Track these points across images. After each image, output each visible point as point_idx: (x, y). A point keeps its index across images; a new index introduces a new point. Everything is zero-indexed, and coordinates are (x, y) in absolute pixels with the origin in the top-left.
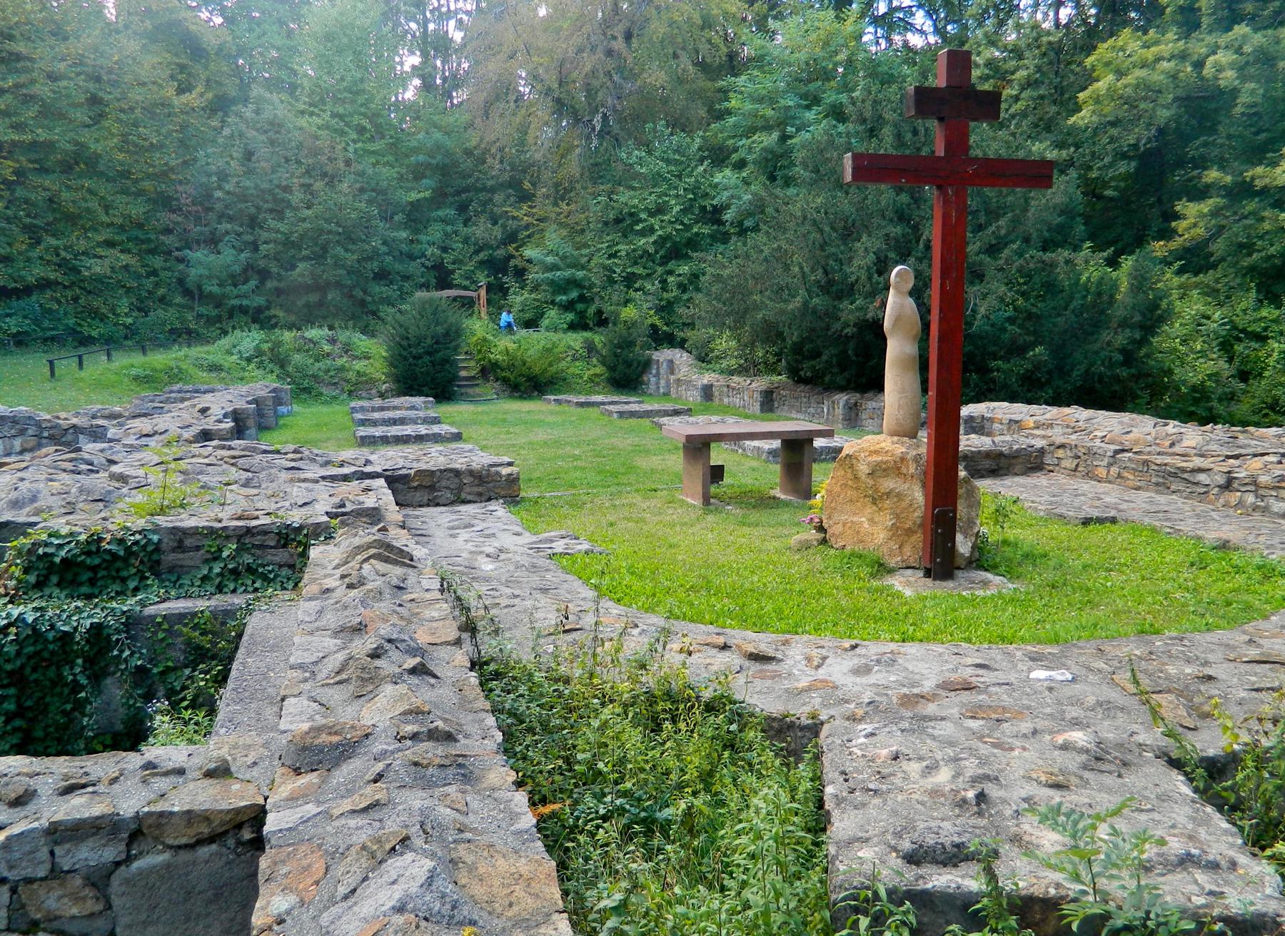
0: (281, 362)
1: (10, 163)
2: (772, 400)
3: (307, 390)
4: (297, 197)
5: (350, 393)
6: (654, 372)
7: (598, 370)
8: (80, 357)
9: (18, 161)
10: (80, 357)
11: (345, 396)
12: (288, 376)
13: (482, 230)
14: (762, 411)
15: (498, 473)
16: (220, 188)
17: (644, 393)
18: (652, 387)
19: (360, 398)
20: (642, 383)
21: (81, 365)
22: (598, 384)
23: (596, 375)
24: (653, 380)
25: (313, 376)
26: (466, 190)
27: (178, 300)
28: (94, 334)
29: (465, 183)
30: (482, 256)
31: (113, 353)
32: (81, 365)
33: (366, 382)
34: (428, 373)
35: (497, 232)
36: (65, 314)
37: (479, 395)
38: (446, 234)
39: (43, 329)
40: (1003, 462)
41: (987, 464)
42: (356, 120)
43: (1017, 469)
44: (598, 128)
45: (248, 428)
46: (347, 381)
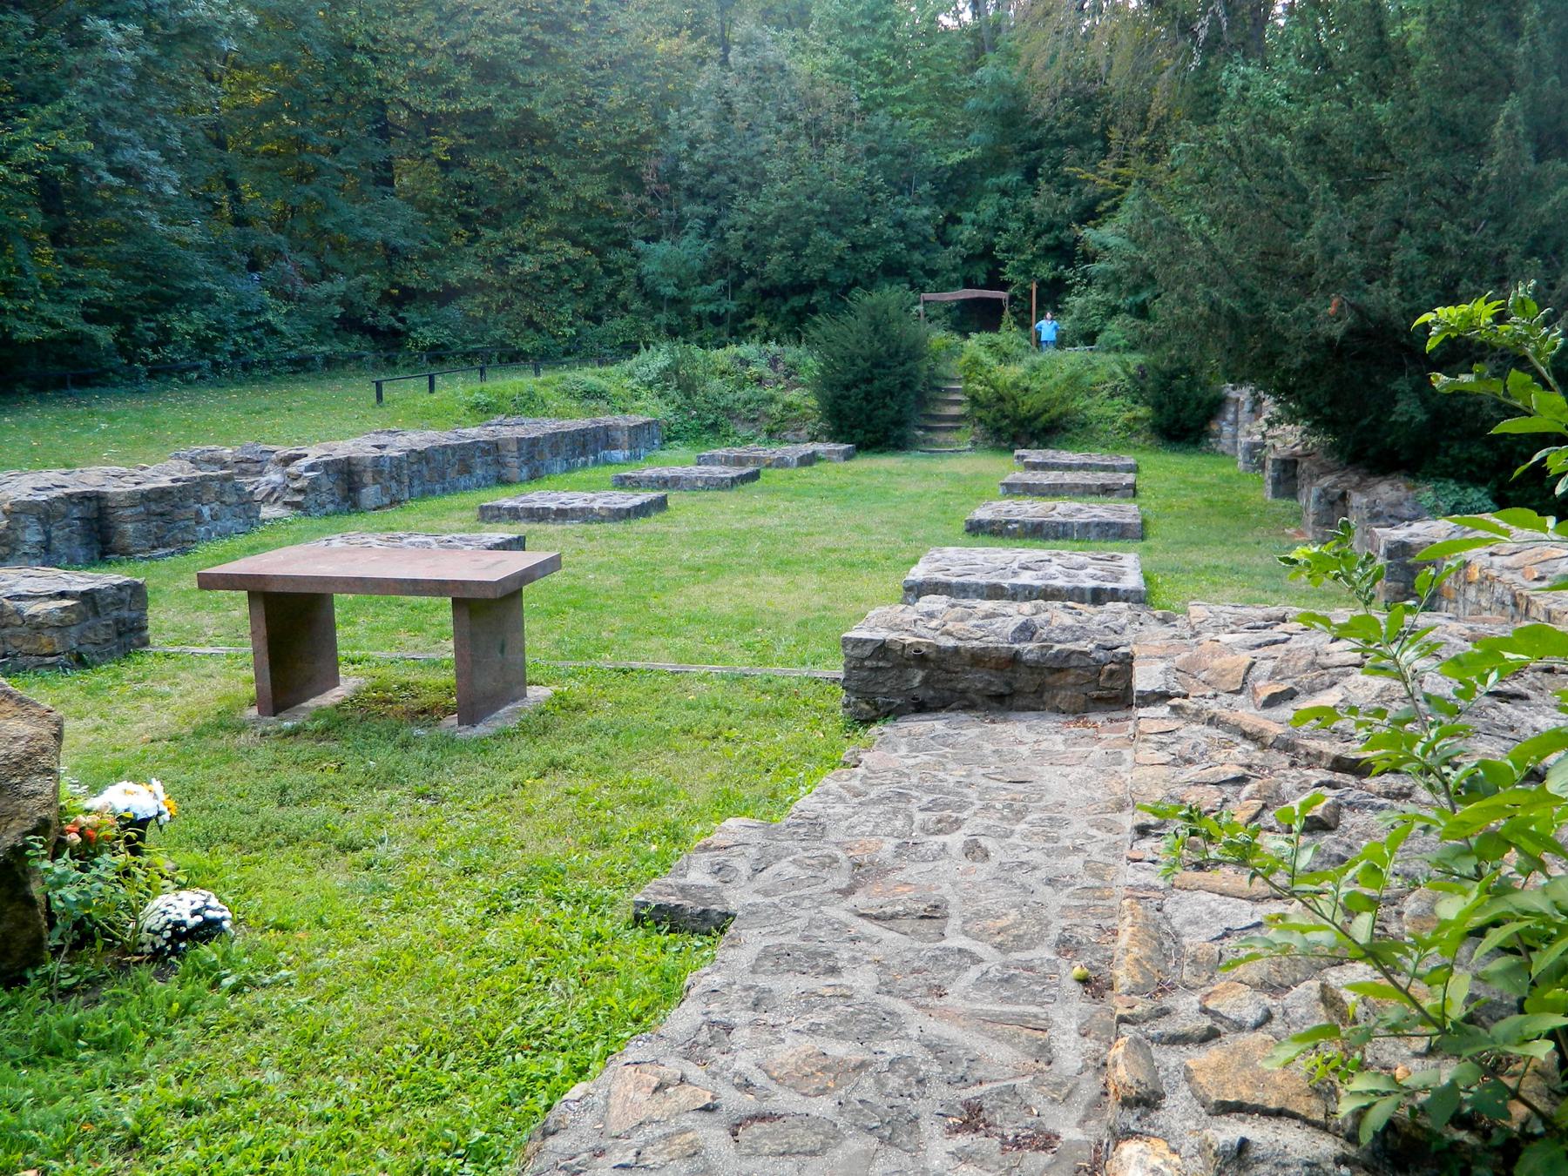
0: (687, 388)
1: (445, 140)
2: (1295, 476)
3: (714, 427)
4: (775, 166)
5: (771, 433)
6: (1230, 417)
7: (1142, 411)
8: (379, 385)
9: (452, 137)
10: (379, 385)
11: (764, 436)
12: (695, 408)
13: (1043, 202)
14: (1276, 494)
15: (18, 612)
16: (689, 158)
17: (1212, 452)
18: (1226, 441)
19: (782, 441)
20: (1208, 435)
21: (432, 389)
22: (1138, 433)
23: (1135, 419)
24: (1227, 430)
25: (725, 409)
26: (1038, 145)
27: (636, 305)
28: (527, 348)
29: (1036, 135)
30: (1045, 240)
31: (438, 380)
32: (432, 389)
33: (795, 420)
34: (861, 409)
35: (1068, 205)
36: (496, 323)
37: (950, 444)
38: (1002, 211)
39: (465, 342)
40: (1024, 680)
41: (976, 680)
42: (876, 55)
43: (1062, 698)
44: (1202, 35)
45: (365, 486)
46: (770, 417)
